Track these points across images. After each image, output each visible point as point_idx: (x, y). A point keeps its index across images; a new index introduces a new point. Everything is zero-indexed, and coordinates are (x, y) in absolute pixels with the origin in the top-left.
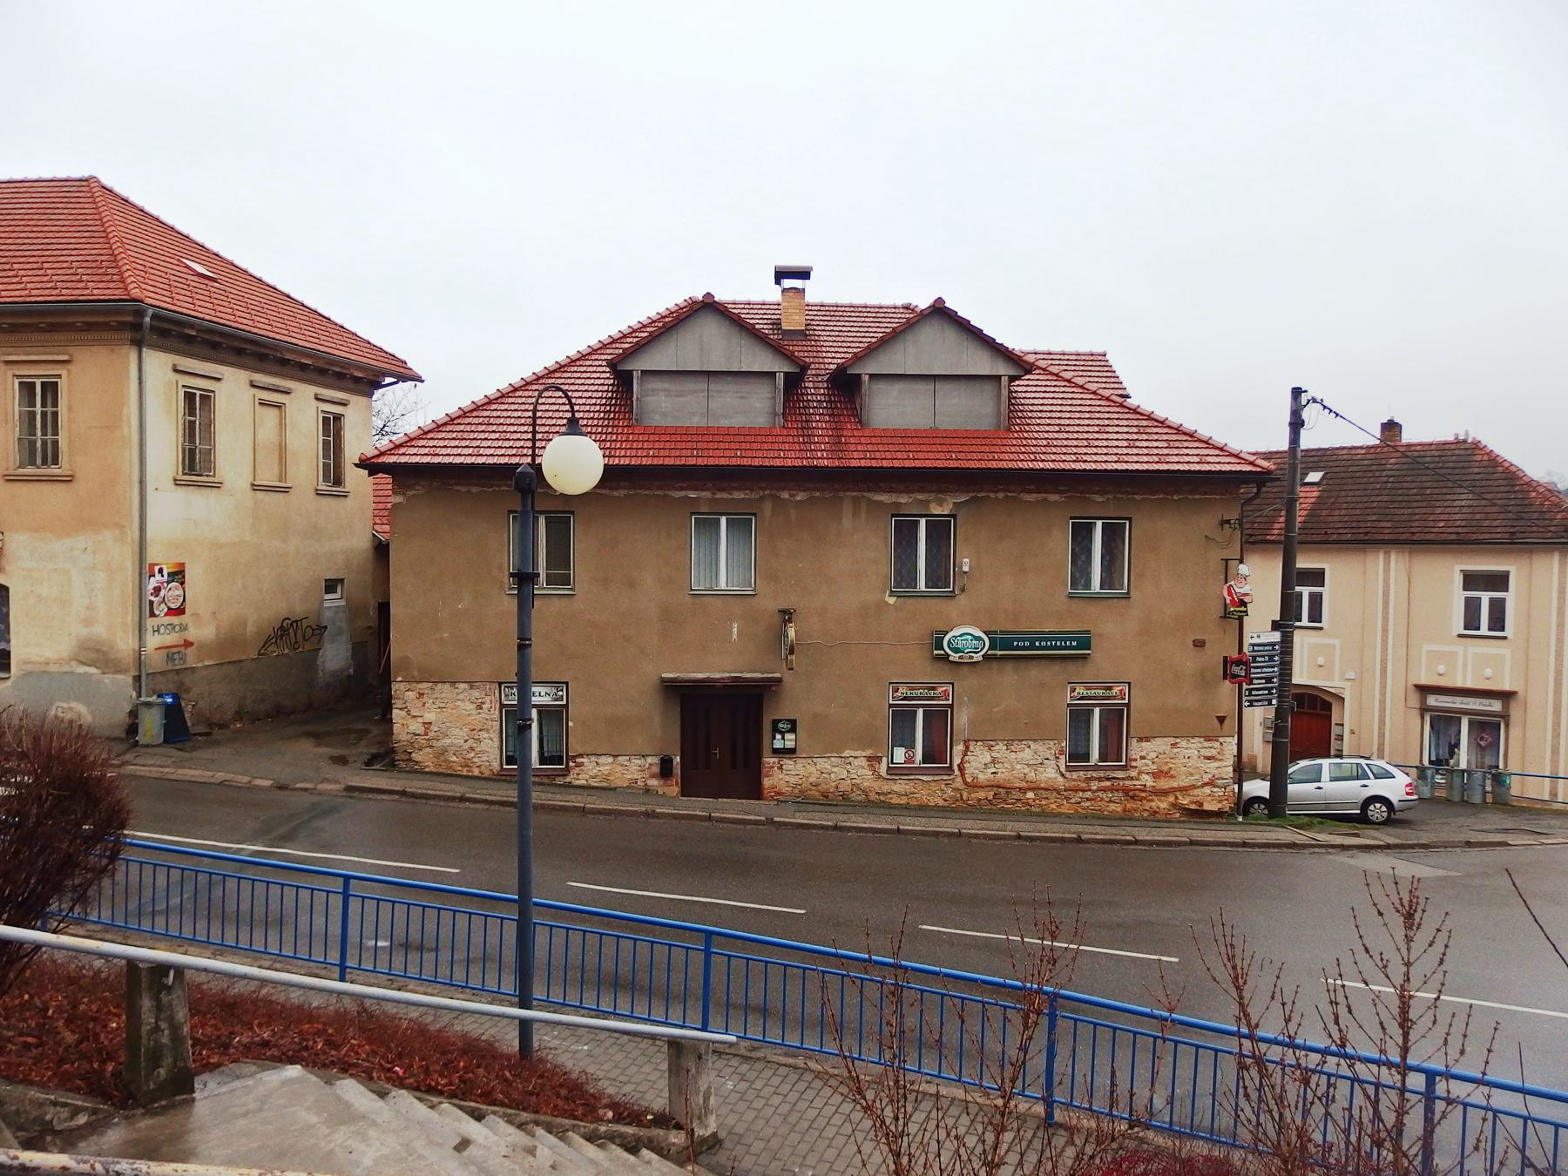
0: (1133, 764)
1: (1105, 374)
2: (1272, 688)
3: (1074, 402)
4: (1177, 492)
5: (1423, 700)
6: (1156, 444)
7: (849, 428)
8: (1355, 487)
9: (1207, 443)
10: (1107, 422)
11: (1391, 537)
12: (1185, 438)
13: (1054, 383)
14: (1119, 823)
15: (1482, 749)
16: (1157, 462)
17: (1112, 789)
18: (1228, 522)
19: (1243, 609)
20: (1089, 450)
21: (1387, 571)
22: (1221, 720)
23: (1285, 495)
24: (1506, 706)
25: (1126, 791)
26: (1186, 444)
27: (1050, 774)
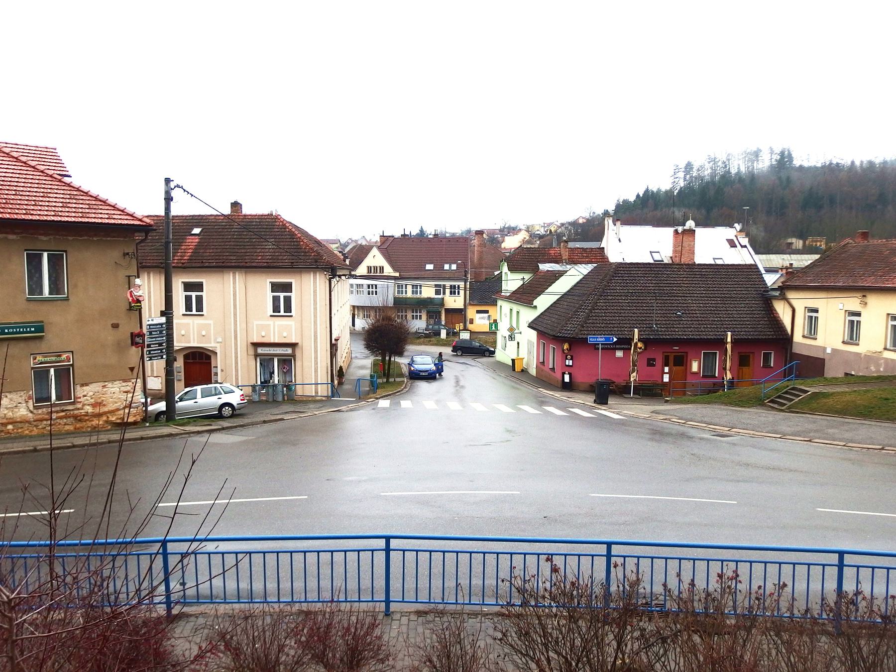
0: (79, 400)
1: (55, 161)
2: (163, 349)
3: (28, 176)
4: (96, 235)
5: (256, 351)
6: (81, 206)
8: (218, 237)
9: (114, 207)
10: (49, 191)
11: (236, 264)
12: (100, 203)
13: (14, 163)
14: (65, 436)
15: (285, 373)
16: (81, 217)
17: (65, 417)
18: (128, 254)
19: (139, 304)
20: (36, 208)
21: (234, 283)
22: (132, 369)
23: (163, 241)
24: (294, 351)
25: (76, 417)
26: (101, 207)
27: (23, 412)
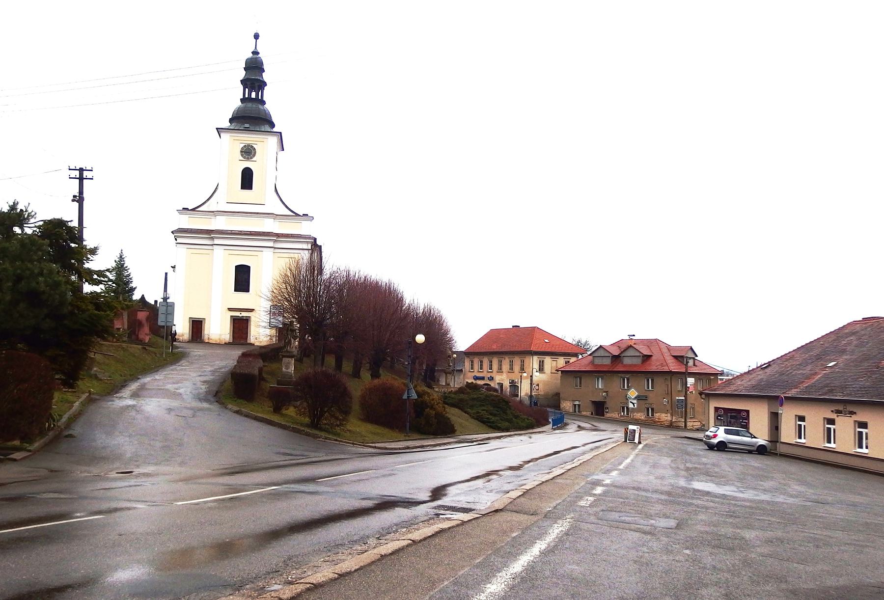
7: (147, 387)
